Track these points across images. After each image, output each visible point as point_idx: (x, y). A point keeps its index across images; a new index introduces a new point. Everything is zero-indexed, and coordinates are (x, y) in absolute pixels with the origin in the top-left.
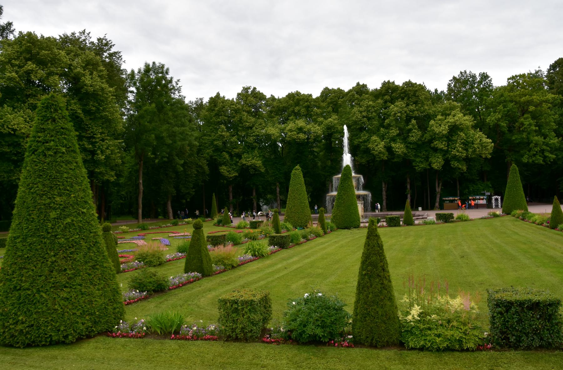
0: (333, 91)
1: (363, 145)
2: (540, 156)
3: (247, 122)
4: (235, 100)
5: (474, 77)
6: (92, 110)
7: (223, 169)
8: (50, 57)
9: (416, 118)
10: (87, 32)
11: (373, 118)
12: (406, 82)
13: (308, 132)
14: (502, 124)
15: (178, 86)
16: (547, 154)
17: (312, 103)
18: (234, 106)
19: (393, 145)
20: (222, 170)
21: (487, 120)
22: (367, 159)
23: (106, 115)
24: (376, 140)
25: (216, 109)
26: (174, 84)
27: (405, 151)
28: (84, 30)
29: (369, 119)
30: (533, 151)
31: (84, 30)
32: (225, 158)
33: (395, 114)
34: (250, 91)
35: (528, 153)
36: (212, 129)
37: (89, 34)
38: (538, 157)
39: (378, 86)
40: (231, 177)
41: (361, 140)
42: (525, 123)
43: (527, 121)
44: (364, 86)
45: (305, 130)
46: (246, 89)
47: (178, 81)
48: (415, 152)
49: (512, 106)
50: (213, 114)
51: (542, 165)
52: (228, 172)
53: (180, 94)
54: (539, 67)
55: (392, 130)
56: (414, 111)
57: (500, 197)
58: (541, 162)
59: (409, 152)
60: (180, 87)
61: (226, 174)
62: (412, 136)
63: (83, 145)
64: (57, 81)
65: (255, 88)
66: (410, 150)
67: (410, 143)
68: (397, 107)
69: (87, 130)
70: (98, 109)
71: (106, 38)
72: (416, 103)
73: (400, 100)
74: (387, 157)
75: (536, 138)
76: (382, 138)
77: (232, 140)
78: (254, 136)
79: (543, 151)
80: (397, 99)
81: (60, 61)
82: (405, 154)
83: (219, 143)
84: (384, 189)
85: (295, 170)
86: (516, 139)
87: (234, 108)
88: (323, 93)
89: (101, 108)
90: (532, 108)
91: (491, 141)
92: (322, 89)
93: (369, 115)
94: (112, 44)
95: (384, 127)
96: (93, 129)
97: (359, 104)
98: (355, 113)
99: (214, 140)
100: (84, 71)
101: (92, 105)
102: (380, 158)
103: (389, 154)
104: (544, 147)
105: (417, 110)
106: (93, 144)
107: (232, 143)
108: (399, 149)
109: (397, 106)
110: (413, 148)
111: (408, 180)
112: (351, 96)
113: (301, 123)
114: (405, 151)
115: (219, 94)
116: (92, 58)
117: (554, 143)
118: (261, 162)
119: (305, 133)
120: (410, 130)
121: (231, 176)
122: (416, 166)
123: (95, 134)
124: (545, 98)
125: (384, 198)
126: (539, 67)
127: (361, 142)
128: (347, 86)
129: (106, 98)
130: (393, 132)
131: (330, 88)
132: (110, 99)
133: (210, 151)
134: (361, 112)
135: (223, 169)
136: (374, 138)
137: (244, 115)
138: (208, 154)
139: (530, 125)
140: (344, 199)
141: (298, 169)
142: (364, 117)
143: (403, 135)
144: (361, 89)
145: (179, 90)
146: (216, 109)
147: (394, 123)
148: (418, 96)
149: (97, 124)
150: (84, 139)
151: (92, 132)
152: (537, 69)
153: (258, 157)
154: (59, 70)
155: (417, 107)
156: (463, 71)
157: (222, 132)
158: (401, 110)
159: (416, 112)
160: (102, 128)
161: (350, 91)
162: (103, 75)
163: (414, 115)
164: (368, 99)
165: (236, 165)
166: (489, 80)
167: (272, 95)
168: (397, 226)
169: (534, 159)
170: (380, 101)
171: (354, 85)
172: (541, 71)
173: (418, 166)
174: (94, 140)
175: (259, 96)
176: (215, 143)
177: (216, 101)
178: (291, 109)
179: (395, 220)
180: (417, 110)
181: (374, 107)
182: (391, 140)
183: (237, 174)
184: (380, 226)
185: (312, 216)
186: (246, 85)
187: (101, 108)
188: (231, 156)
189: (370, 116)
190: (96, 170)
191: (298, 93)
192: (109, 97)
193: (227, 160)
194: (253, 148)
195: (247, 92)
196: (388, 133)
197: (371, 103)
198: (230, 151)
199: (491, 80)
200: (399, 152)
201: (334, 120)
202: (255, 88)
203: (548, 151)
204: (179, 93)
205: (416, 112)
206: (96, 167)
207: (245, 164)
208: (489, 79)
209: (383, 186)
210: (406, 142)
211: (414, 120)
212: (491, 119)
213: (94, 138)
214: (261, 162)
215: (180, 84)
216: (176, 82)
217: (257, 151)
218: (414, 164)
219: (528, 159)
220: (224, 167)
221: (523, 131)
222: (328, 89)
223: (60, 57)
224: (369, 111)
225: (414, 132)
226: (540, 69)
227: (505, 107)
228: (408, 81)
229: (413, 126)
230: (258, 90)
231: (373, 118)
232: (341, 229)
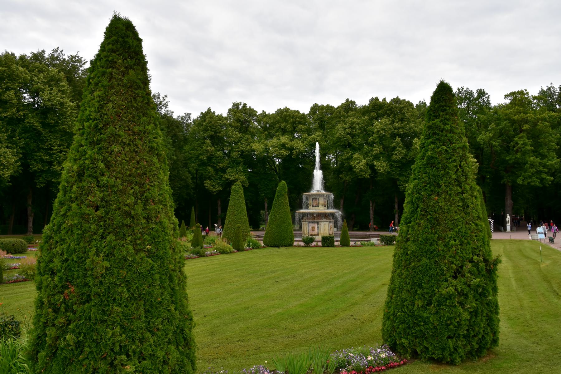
0: (322, 107)
1: (346, 163)
2: (537, 178)
3: (232, 137)
4: (258, 114)
5: (471, 93)
6: (51, 123)
7: (207, 183)
8: (7, 74)
9: (400, 136)
10: (60, 49)
11: (358, 136)
12: (394, 99)
13: (291, 149)
14: (494, 143)
15: (165, 101)
16: (544, 176)
17: (297, 119)
18: (220, 122)
19: (375, 163)
20: (206, 184)
21: (478, 139)
22: (351, 177)
23: (64, 128)
24: (358, 157)
25: (205, 124)
26: (162, 99)
27: (388, 169)
28: (58, 48)
29: (353, 136)
30: (528, 172)
31: (58, 48)
32: (209, 173)
33: (378, 131)
34: (240, 107)
35: (523, 174)
36: (199, 144)
37: (61, 52)
38: (534, 179)
39: (366, 102)
40: (215, 192)
41: (344, 158)
42: (519, 142)
43: (522, 140)
44: (353, 103)
45: (288, 146)
46: (236, 105)
47: (166, 96)
48: (400, 170)
49: (505, 124)
50: (201, 128)
51: (538, 188)
52: (213, 186)
53: (168, 109)
54: (552, 84)
55: (376, 147)
56: (399, 128)
57: (493, 220)
58: (538, 184)
59: (393, 171)
60: (167, 102)
61: (210, 188)
62: (396, 154)
63: (40, 156)
64: (12, 95)
65: (245, 104)
66: (394, 169)
67: (394, 162)
68: (380, 124)
69: (46, 142)
70: (57, 122)
71: (79, 55)
72: (402, 120)
73: (385, 117)
74: (370, 175)
75: (531, 158)
76: (366, 155)
77: (216, 155)
78: (239, 151)
79: (539, 172)
80: (383, 115)
81: (18, 77)
82: (388, 173)
83: (204, 158)
84: (371, 208)
85: (236, 185)
86: (510, 159)
87: (220, 123)
88: (312, 109)
89: (60, 121)
90: (526, 127)
91: (475, 160)
92: (312, 105)
93: (353, 132)
94: (86, 61)
95: (367, 143)
96: (51, 141)
97: (345, 121)
98: (338, 130)
99: (200, 154)
100: (43, 86)
101: (51, 119)
102: (361, 176)
103: (372, 173)
104: (541, 168)
105: (402, 128)
106: (51, 155)
107: (217, 157)
108: (381, 167)
109: (381, 123)
110: (397, 167)
111: (396, 200)
112: (338, 112)
113: (284, 139)
114: (388, 169)
115: (211, 110)
116: (54, 74)
117: (551, 165)
118: (245, 177)
119: (286, 149)
120: (394, 148)
121: (215, 190)
122: (400, 185)
123: (53, 146)
124: (542, 115)
125: (371, 218)
126: (552, 84)
127: (345, 160)
128: (336, 102)
129: (65, 113)
130: (376, 150)
131: (320, 104)
132: (68, 113)
133: (193, 166)
134: (345, 129)
135: (208, 184)
136: (356, 155)
137: (230, 131)
138: (193, 168)
139: (525, 144)
140: (276, 216)
141: (239, 185)
142: (348, 134)
143: (388, 152)
144: (349, 106)
145: (166, 105)
146: (205, 124)
147: (378, 140)
148: (404, 114)
149: (57, 137)
150: (42, 150)
151: (50, 144)
152: (550, 86)
153: (242, 172)
154: (16, 86)
155: (403, 125)
156: (460, 88)
157: (207, 147)
158: (385, 127)
159: (401, 130)
160: (62, 140)
161: (339, 107)
162: (64, 90)
163: (399, 133)
164: (354, 115)
165: (220, 179)
166: (486, 97)
167: (263, 111)
168: (390, 245)
169: (530, 181)
170: (366, 118)
171: (344, 101)
172: (553, 87)
173: (402, 185)
174: (51, 152)
175: (251, 112)
176: (201, 157)
177: (208, 115)
178: (278, 125)
179: (329, 240)
180: (402, 128)
181: (358, 124)
182: (375, 158)
183: (221, 189)
184: (315, 245)
185: (349, 232)
186: (237, 100)
187: (60, 121)
188: (216, 170)
189: (354, 133)
190: (53, 180)
191: (287, 110)
192: (69, 110)
193: (212, 174)
194: (238, 164)
195: (238, 108)
196: (372, 150)
197: (355, 120)
198: (215, 165)
199: (488, 97)
200: (380, 170)
201: (318, 136)
202: (245, 104)
203: (546, 173)
204: (166, 108)
205: (401, 130)
206: (54, 178)
207: (228, 179)
208: (487, 96)
209: (371, 205)
210: (389, 161)
211: (399, 138)
212: (482, 137)
213: (52, 150)
214: (245, 177)
215: (167, 99)
216: (163, 98)
217: (242, 166)
218: (398, 183)
219: (523, 180)
220: (208, 181)
221: (517, 151)
222: (318, 105)
223: (17, 73)
224: (354, 128)
225: (398, 150)
226: (552, 86)
227: (498, 125)
228: (396, 97)
229: (397, 143)
230: (248, 106)
231: (358, 136)
232: (270, 246)
